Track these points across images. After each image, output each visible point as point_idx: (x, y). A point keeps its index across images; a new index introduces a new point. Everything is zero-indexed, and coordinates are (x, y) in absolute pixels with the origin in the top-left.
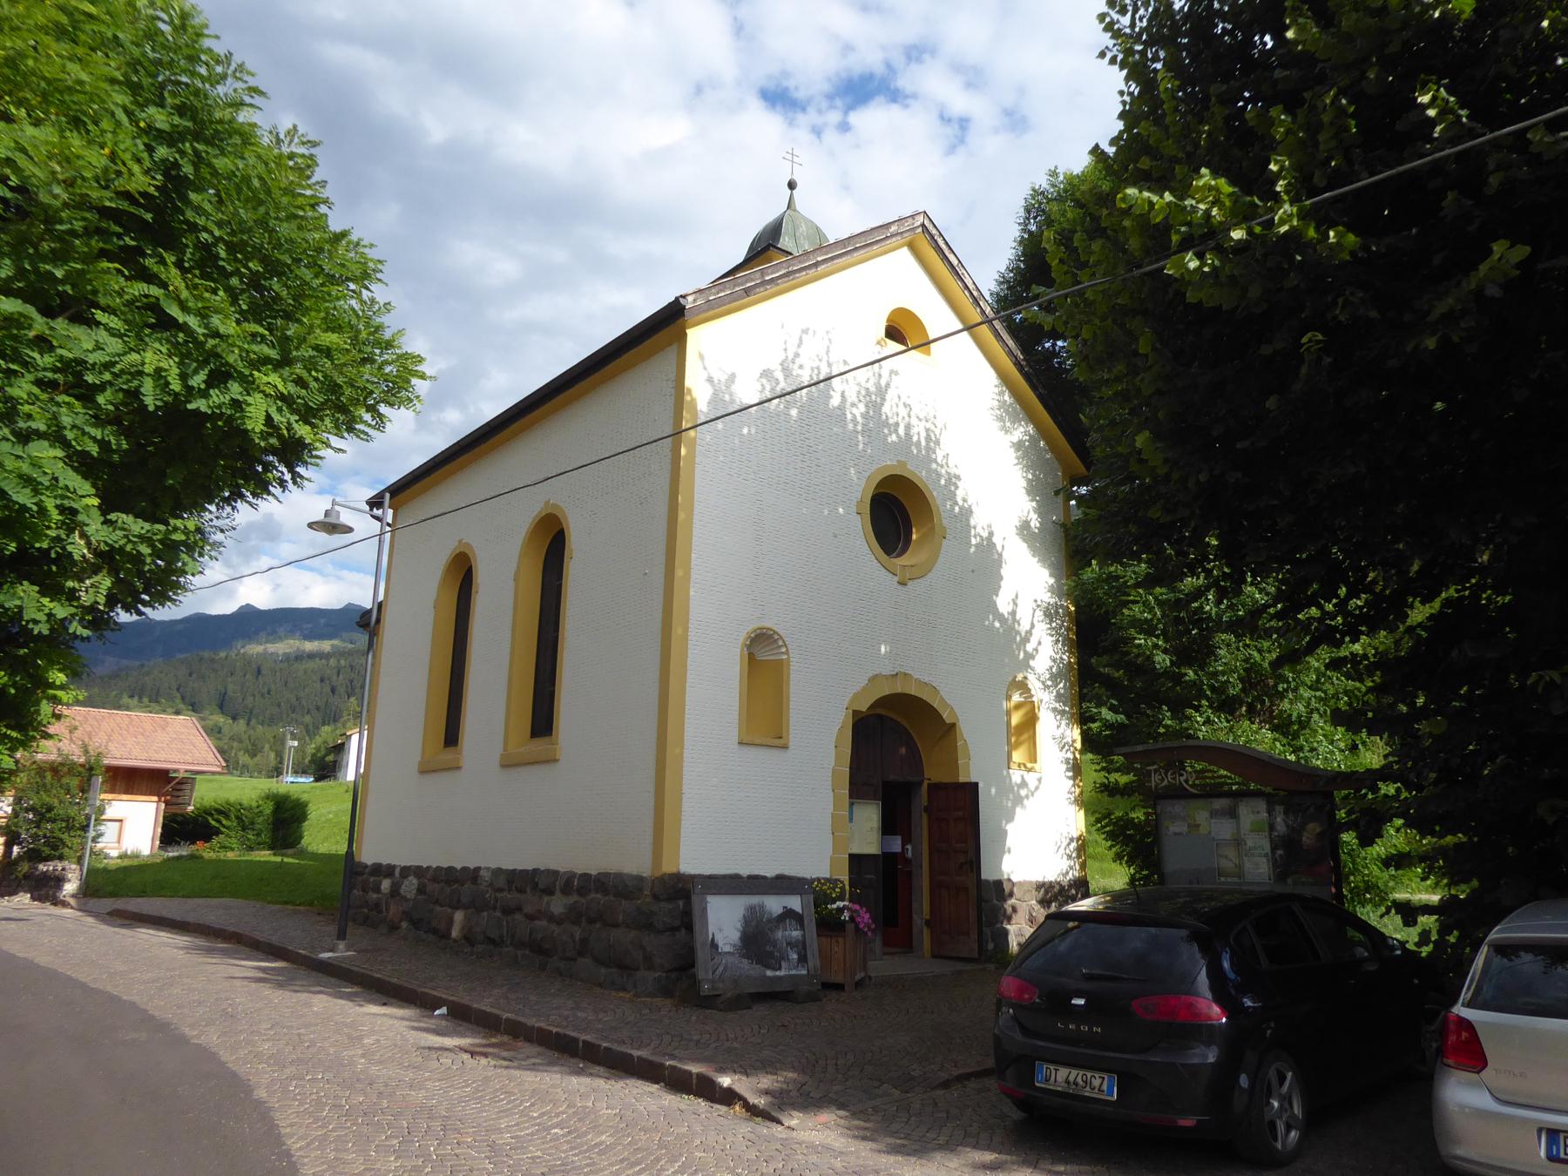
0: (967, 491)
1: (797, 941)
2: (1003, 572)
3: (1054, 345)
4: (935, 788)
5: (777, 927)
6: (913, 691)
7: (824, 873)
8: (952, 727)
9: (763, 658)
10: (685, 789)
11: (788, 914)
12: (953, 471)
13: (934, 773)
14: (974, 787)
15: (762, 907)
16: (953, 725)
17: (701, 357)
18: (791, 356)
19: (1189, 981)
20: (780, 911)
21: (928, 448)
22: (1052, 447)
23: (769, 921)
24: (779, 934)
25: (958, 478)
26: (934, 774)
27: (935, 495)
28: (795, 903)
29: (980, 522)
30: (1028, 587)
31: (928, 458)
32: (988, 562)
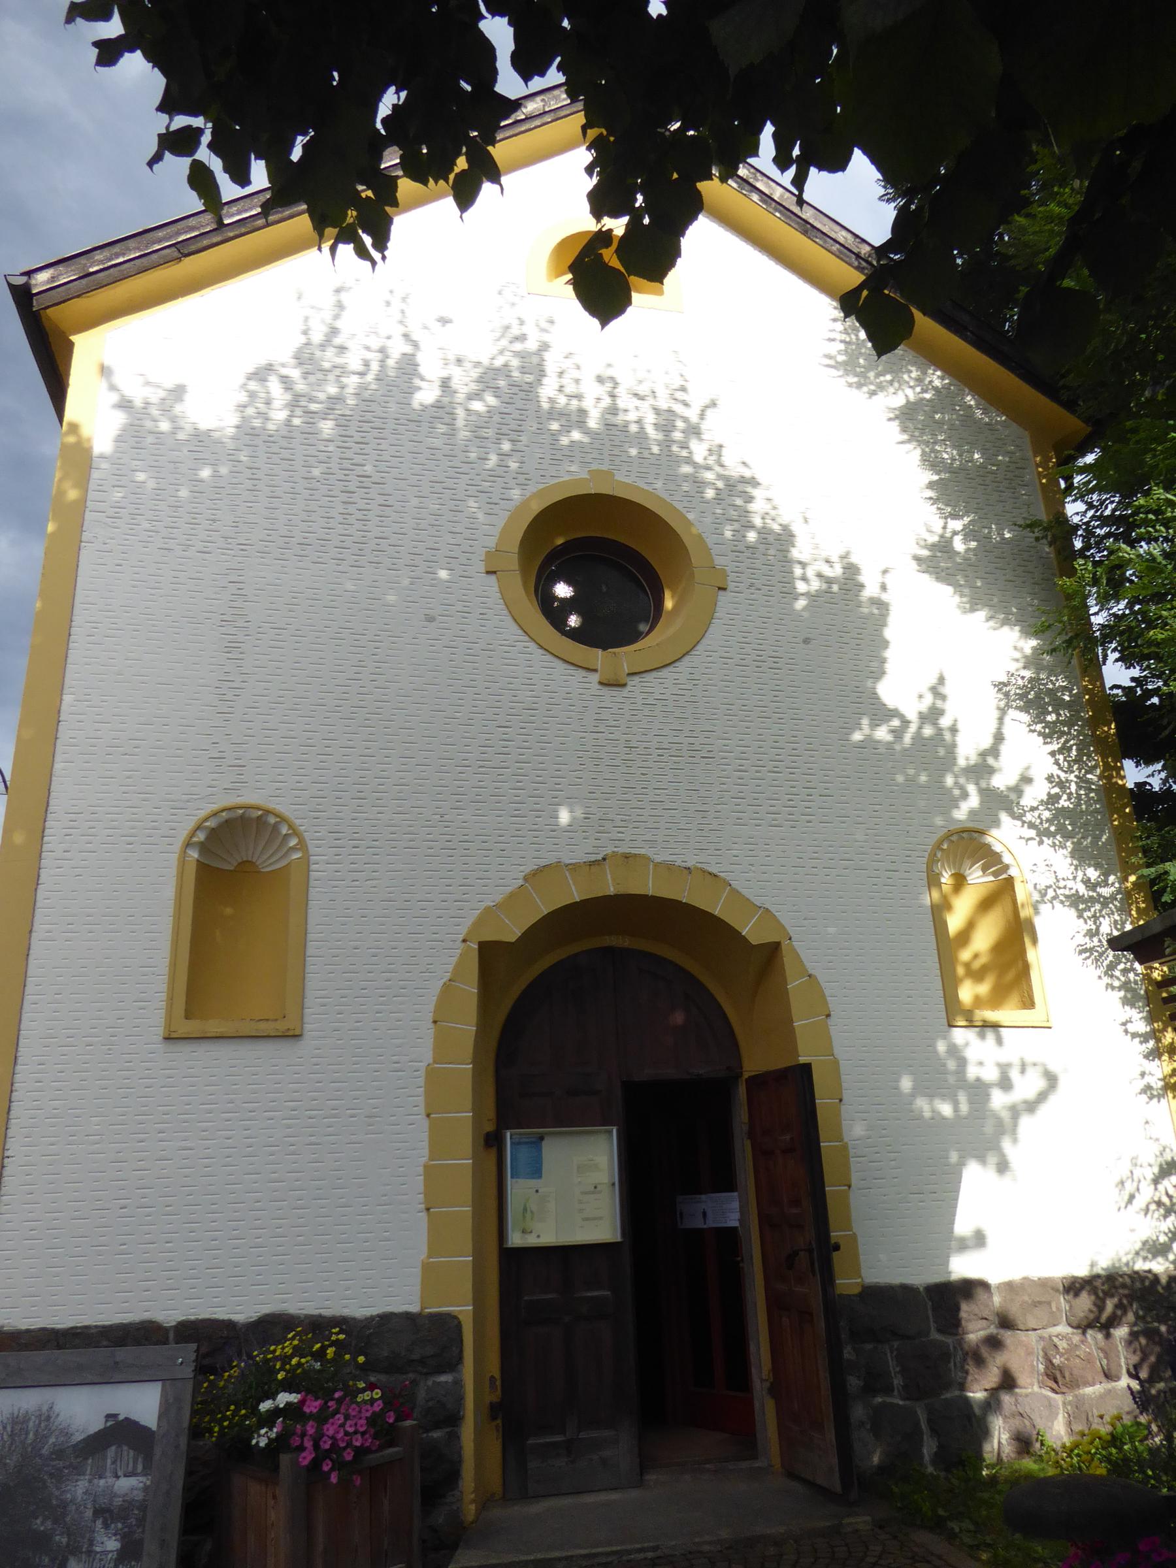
0: (777, 501)
1: (128, 1506)
2: (888, 633)
3: (1117, 529)
4: (759, 1082)
5: (78, 1470)
6: (650, 886)
7: (400, 1294)
8: (770, 957)
9: (235, 874)
10: (14, 1147)
11: (121, 1433)
12: (735, 470)
13: (756, 1060)
14: (807, 1068)
15: (46, 1417)
16: (773, 950)
17: (105, 371)
18: (317, 337)
19: (902, 296)
20: (96, 1424)
21: (667, 443)
22: (991, 397)
23: (59, 1453)
24: (79, 1488)
25: (753, 482)
26: (755, 1062)
27: (695, 521)
28: (143, 1403)
29: (816, 552)
30: (959, 666)
31: (669, 458)
32: (849, 622)
